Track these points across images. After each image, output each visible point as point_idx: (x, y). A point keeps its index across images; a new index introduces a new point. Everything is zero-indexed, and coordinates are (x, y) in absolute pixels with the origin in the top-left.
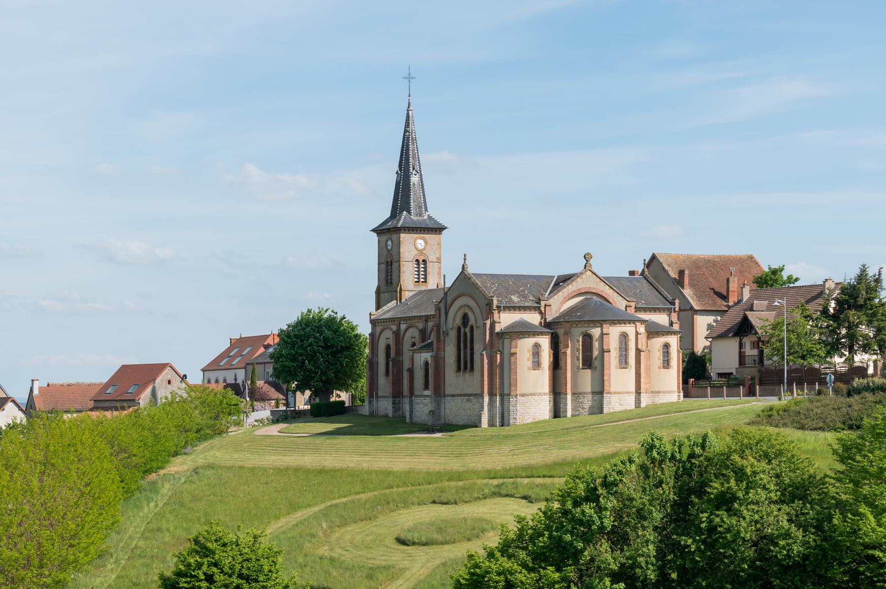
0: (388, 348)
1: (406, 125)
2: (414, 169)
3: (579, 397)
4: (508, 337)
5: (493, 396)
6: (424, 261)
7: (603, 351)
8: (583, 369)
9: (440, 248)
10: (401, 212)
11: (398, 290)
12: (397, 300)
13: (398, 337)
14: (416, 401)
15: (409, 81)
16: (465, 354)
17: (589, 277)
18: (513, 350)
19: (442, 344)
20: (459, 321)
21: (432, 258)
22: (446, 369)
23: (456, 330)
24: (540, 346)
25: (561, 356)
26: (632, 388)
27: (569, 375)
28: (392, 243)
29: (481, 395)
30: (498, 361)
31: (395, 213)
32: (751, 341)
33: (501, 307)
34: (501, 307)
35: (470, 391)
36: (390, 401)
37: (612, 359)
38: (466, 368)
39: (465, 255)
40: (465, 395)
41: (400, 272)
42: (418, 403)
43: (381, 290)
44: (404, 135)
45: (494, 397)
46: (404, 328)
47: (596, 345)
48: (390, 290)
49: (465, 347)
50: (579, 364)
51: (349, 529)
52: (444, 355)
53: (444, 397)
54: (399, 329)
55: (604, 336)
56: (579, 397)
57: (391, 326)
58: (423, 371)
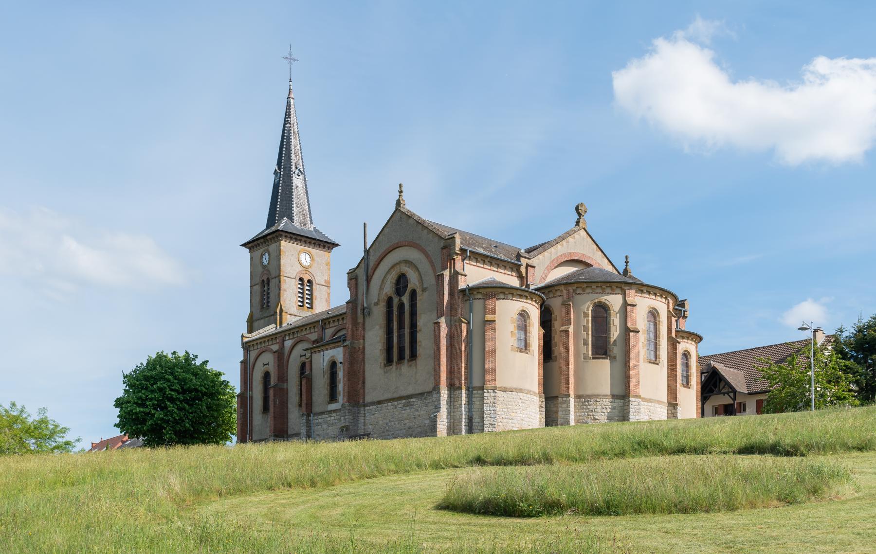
0: (267, 376)
1: (286, 115)
2: (296, 168)
4: (480, 296)
5: (454, 390)
6: (309, 281)
7: (627, 331)
8: (593, 358)
9: (329, 269)
10: (281, 218)
11: (278, 311)
12: (276, 324)
13: (281, 358)
14: (316, 421)
15: (290, 63)
16: (401, 337)
17: (583, 238)
18: (489, 317)
19: (361, 330)
20: (389, 289)
21: (319, 279)
22: (367, 365)
23: (385, 304)
24: (529, 316)
25: (556, 338)
26: (664, 396)
27: (571, 367)
29: (437, 389)
30: (464, 334)
31: (271, 221)
32: (713, 406)
33: (466, 250)
34: (466, 250)
35: (410, 391)
37: (640, 344)
38: (401, 358)
39: (400, 185)
40: (400, 398)
41: (280, 289)
42: (318, 424)
43: (254, 318)
44: (284, 127)
45: (457, 392)
46: (290, 344)
47: (615, 322)
48: (266, 315)
49: (401, 326)
50: (587, 350)
51: (253, 499)
52: (364, 343)
53: (365, 405)
54: (282, 346)
55: (628, 307)
58: (327, 376)
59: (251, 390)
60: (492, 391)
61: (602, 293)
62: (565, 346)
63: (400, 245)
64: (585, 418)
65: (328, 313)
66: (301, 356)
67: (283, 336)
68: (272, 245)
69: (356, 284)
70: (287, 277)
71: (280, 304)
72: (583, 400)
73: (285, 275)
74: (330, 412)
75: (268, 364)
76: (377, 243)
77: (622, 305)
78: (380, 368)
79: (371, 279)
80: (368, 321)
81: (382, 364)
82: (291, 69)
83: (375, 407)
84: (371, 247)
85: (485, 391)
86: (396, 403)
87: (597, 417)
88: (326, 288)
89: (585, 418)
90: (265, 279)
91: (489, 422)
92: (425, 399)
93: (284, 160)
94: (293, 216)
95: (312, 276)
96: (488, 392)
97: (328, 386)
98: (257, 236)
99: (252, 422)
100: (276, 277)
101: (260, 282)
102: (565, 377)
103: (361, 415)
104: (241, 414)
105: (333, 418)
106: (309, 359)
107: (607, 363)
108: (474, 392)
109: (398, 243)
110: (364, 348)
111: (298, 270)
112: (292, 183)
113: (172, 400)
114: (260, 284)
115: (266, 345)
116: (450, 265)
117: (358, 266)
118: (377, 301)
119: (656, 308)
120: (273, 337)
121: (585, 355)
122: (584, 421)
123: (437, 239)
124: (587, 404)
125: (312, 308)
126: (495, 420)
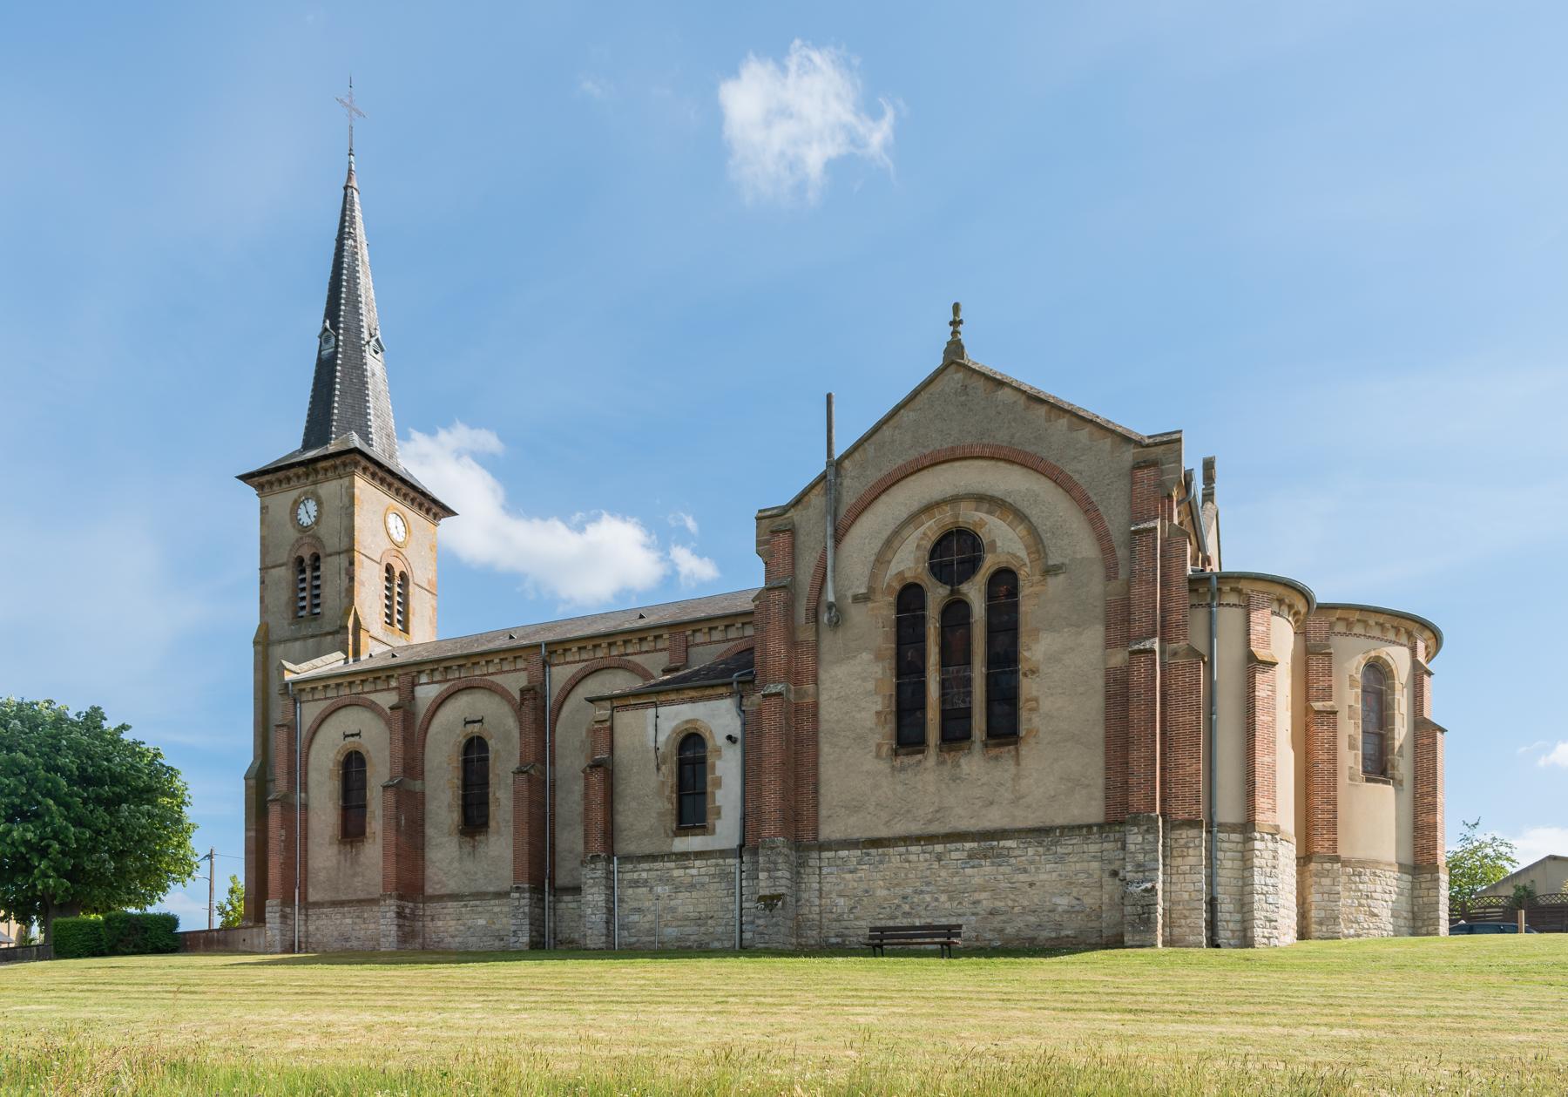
3: (1360, 875)
12: (346, 653)
14: (628, 876)
20: (909, 561)
23: (892, 599)
28: (319, 511)
35: (994, 819)
36: (389, 909)
52: (817, 694)
56: (1360, 875)
57: (373, 697)
59: (305, 787)
60: (1270, 836)
61: (1394, 642)
62: (1327, 746)
63: (957, 455)
64: (1353, 910)
65: (511, 637)
66: (467, 723)
67: (415, 674)
69: (793, 546)
70: (366, 556)
71: (353, 612)
72: (1351, 870)
73: (362, 552)
74: (685, 855)
75: (358, 734)
76: (870, 448)
77: (1410, 672)
78: (878, 756)
79: (844, 535)
80: (830, 642)
81: (885, 750)
82: (351, 128)
83: (858, 852)
84: (848, 455)
85: (1257, 835)
86: (939, 848)
87: (1376, 911)
88: (430, 595)
89: (1353, 910)
91: (1265, 914)
92: (1056, 843)
93: (344, 311)
94: (371, 433)
95: (408, 567)
96: (1262, 839)
97: (672, 792)
98: (280, 460)
99: (306, 862)
100: (339, 553)
101: (292, 560)
102: (1326, 816)
103: (809, 870)
105: (694, 872)
106: (608, 724)
107: (1389, 790)
108: (1221, 835)
109: (953, 449)
110: (816, 705)
111: (384, 548)
112: (366, 364)
114: (291, 565)
115: (354, 691)
116: (1163, 511)
117: (797, 502)
118: (863, 590)
119: (461, 749)
120: (303, 686)
121: (1352, 771)
122: (1351, 916)
123: (1107, 443)
124: (1358, 880)
125: (406, 630)
126: (1276, 910)
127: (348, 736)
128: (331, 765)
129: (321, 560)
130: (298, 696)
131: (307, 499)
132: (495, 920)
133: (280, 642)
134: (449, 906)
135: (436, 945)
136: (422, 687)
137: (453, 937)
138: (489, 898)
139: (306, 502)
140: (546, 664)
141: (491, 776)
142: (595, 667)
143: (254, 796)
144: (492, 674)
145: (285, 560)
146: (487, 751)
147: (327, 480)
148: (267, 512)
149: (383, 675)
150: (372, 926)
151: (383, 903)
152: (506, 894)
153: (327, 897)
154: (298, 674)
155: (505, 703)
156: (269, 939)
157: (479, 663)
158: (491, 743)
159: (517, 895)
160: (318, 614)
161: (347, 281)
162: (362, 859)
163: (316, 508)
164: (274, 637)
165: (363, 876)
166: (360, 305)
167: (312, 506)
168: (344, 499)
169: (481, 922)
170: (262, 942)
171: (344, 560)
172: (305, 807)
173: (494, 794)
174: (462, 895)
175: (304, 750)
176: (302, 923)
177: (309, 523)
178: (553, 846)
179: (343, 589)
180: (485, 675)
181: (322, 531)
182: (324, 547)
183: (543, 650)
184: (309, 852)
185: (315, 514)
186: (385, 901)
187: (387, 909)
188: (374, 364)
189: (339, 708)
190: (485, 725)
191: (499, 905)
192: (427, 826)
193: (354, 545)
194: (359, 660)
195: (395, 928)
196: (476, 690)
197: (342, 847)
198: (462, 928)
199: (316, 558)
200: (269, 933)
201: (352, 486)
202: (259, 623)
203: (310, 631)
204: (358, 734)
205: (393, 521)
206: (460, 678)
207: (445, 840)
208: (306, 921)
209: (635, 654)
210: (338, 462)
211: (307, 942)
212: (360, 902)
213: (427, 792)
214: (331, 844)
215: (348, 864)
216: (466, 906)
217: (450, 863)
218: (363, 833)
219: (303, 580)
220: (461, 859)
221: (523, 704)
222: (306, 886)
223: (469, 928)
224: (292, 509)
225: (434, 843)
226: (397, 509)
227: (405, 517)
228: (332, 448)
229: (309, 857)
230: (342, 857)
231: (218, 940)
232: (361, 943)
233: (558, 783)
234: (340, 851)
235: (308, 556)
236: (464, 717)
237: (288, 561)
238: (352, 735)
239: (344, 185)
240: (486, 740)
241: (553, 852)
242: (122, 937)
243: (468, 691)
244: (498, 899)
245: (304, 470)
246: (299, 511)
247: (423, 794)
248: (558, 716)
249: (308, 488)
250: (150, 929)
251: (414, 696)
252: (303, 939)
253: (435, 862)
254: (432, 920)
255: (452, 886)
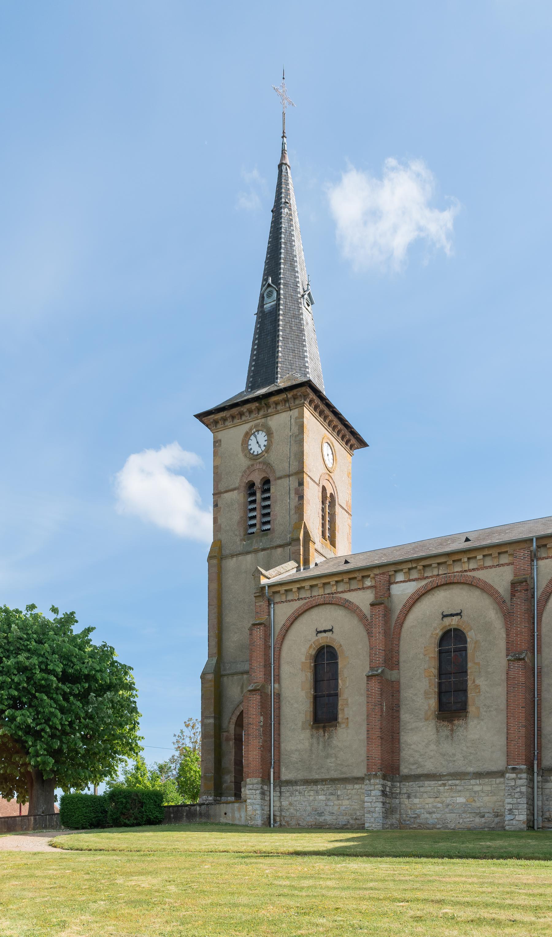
57: (347, 596)
66: (444, 616)
68: (276, 417)
70: (311, 478)
75: (331, 630)
82: (284, 114)
90: (257, 479)
100: (289, 476)
101: (243, 485)
104: (261, 726)
113: (46, 689)
114: (242, 489)
119: (437, 641)
127: (321, 632)
128: (303, 660)
129: (272, 483)
130: (272, 598)
131: (258, 431)
132: (476, 799)
133: (232, 556)
134: (426, 785)
135: (412, 820)
136: (398, 585)
137: (430, 813)
138: (469, 778)
139: (256, 433)
140: (534, 557)
141: (470, 665)
142: (314, 603)
143: (213, 689)
144: (474, 570)
145: (237, 485)
146: (465, 642)
147: (278, 412)
148: (220, 445)
149: (359, 575)
150: (346, 802)
151: (368, 781)
152: (501, 774)
153: (300, 776)
154: (269, 578)
155: (485, 596)
156: (250, 813)
157: (460, 560)
158: (471, 636)
159: (513, 776)
160: (269, 530)
161: (285, 243)
162: (335, 742)
163: (266, 438)
164: (226, 552)
165: (336, 757)
166: (296, 264)
167: (262, 437)
168: (293, 427)
169: (461, 800)
170: (242, 815)
171: (293, 482)
172: (278, 696)
173: (474, 682)
174: (440, 775)
175: (278, 646)
176: (277, 799)
177: (260, 452)
178: (540, 729)
179: (293, 507)
180: (466, 571)
181: (273, 458)
182: (274, 472)
183: (535, 544)
184: (282, 736)
185: (266, 443)
186: (370, 780)
187: (372, 788)
188: (307, 315)
189: (313, 607)
190: (465, 618)
191: (480, 784)
192: (402, 712)
193: (303, 468)
194: (309, 568)
195: (380, 805)
196: (454, 586)
197: (315, 732)
198: (439, 805)
199: (266, 482)
200: (250, 808)
201: (302, 416)
202: (212, 540)
203: (261, 545)
204: (331, 630)
205: (327, 450)
206: (438, 575)
207: (421, 724)
208: (280, 796)
209: (477, 569)
210: (290, 395)
211: (281, 816)
212: (333, 781)
213: (402, 681)
214: (303, 729)
215: (321, 747)
216: (444, 785)
217: (428, 745)
218: (335, 718)
219: (254, 502)
220: (438, 743)
221: (514, 595)
222: (279, 766)
223: (448, 805)
224: (243, 441)
225: (410, 728)
226: (330, 440)
227: (333, 447)
228: (281, 383)
229: (282, 740)
230: (315, 740)
231: (200, 814)
232: (334, 817)
233: (545, 670)
234: (312, 735)
235: (259, 481)
236: (441, 611)
237: (240, 486)
238: (325, 631)
239: (278, 163)
240: (465, 631)
241: (540, 735)
242: (125, 811)
243: (445, 587)
244: (480, 778)
245: (257, 405)
246: (250, 442)
247: (398, 682)
248: (545, 606)
249: (259, 421)
250: (145, 803)
251: (390, 593)
252: (278, 813)
253: (411, 745)
254: (409, 797)
255: (429, 767)
